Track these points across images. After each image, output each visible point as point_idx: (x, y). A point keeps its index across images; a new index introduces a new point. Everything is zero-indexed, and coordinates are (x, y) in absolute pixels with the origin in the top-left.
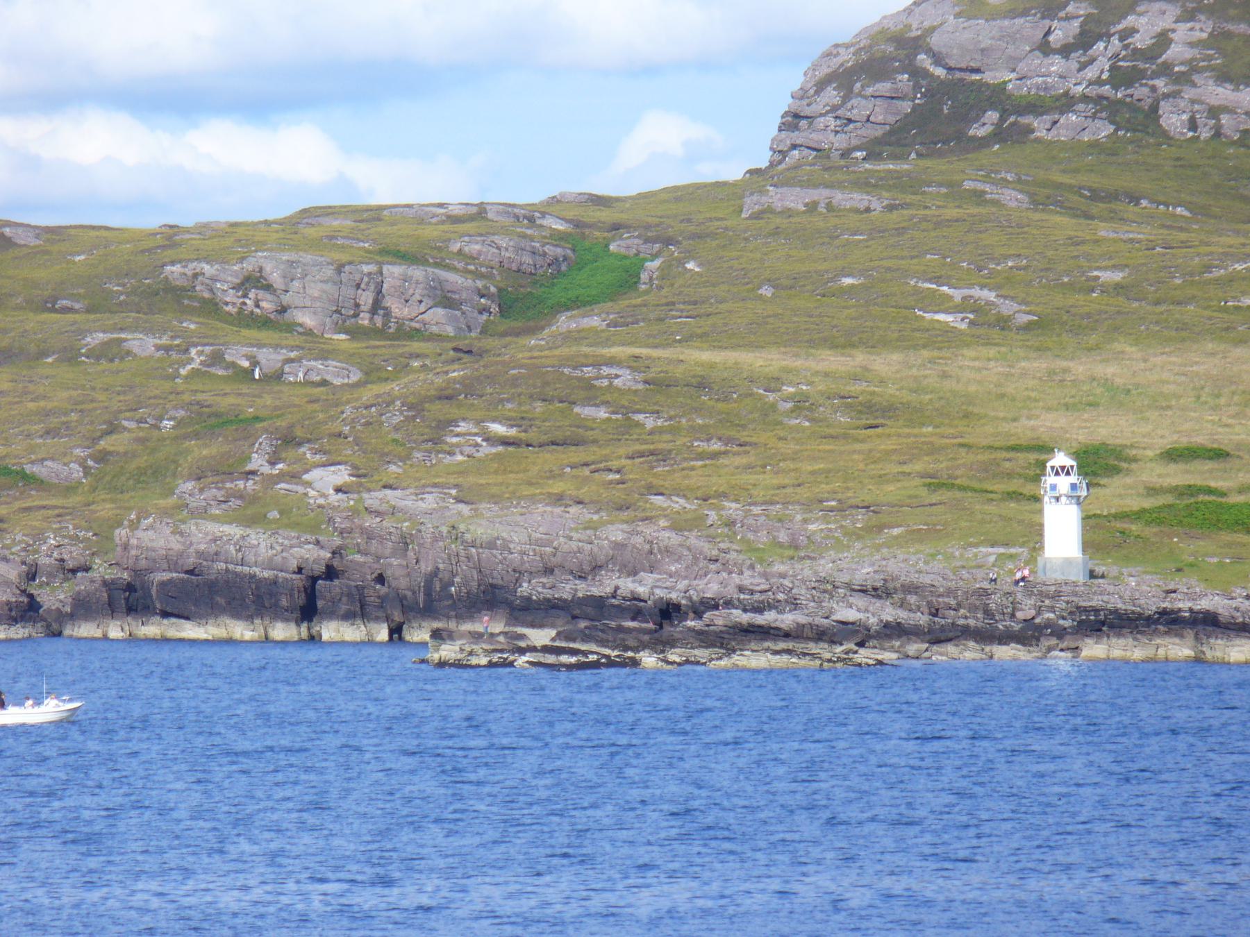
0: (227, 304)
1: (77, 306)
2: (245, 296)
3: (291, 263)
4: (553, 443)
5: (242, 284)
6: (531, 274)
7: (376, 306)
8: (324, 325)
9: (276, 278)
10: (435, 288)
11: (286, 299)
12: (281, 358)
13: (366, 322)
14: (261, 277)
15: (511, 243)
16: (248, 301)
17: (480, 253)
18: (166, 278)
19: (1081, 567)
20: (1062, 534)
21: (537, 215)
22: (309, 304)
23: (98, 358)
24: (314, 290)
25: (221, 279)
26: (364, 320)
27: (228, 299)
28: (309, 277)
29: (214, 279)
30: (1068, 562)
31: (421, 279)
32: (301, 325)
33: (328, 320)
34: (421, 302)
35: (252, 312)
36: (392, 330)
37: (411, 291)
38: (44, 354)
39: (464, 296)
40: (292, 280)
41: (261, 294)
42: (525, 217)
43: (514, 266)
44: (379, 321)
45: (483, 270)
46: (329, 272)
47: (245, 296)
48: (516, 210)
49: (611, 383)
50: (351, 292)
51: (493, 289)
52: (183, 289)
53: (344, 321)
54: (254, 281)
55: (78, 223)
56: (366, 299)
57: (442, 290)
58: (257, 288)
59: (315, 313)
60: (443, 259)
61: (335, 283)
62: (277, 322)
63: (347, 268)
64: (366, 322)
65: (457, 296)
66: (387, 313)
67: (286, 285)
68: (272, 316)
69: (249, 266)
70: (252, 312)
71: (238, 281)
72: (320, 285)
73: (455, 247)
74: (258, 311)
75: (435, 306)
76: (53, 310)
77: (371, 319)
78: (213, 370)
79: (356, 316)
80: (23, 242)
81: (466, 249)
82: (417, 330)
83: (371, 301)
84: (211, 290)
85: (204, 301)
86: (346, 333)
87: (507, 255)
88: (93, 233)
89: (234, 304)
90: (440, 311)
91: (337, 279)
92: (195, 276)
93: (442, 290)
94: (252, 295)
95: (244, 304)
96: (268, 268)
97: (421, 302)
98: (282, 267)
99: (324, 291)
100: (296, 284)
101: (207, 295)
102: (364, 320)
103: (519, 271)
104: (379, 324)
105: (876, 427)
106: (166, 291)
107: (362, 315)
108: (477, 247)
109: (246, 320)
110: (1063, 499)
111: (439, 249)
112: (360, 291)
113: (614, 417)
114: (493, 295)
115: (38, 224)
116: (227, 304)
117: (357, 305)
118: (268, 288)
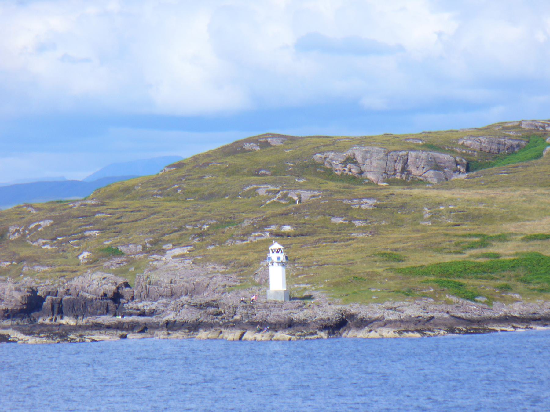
0: (336, 170)
1: (268, 173)
2: (346, 167)
3: (366, 152)
4: (302, 235)
5: (345, 161)
6: (496, 153)
7: (404, 169)
8: (379, 179)
9: (359, 159)
10: (431, 162)
11: (363, 168)
12: (310, 195)
13: (399, 177)
14: (354, 158)
15: (487, 140)
16: (346, 169)
17: (471, 145)
18: (314, 160)
19: (283, 295)
20: (277, 280)
21: (546, 125)
22: (372, 170)
23: (244, 197)
24: (375, 164)
25: (335, 160)
26: (398, 177)
27: (337, 168)
28: (373, 158)
29: (332, 160)
30: (277, 292)
31: (424, 158)
32: (369, 179)
33: (381, 177)
34: (424, 168)
35: (347, 174)
36: (409, 181)
37: (420, 163)
38: (226, 195)
39: (447, 164)
40: (366, 159)
41: (352, 166)
42: (541, 126)
43: (487, 150)
44: (404, 176)
45: (470, 152)
46: (382, 155)
47: (346, 167)
48: (536, 124)
49: (360, 207)
50: (392, 164)
51: (464, 161)
52: (320, 164)
53: (388, 177)
54: (351, 160)
55: (316, 135)
56: (399, 167)
57: (436, 162)
58: (351, 163)
59: (375, 174)
60: (452, 148)
61: (384, 160)
62: (359, 179)
63: (391, 154)
64: (399, 177)
65: (443, 165)
66: (409, 173)
67: (364, 161)
68: (356, 176)
69: (349, 153)
70: (347, 174)
71: (343, 160)
72: (377, 161)
73: (461, 142)
74: (350, 173)
75: (431, 169)
76: (258, 175)
77: (401, 176)
78: (281, 201)
79: (394, 174)
80: (274, 144)
81: (465, 143)
82: (422, 180)
83: (401, 168)
84: (331, 165)
85: (327, 169)
86: (387, 183)
87: (484, 145)
88: (324, 140)
89: (340, 170)
90: (432, 172)
91: (385, 158)
92: (326, 158)
93: (436, 162)
94: (348, 167)
95: (344, 170)
96: (357, 153)
97: (424, 168)
98: (362, 153)
99: (379, 164)
100: (368, 161)
101: (329, 167)
102: (398, 177)
103: (490, 152)
104: (404, 178)
105: (459, 225)
106: (312, 165)
107: (397, 174)
108: (470, 142)
109: (344, 178)
110: (275, 264)
111: (454, 143)
112: (396, 164)
113: (344, 222)
114: (464, 164)
115: (286, 134)
116: (336, 170)
117: (395, 170)
118: (356, 163)
